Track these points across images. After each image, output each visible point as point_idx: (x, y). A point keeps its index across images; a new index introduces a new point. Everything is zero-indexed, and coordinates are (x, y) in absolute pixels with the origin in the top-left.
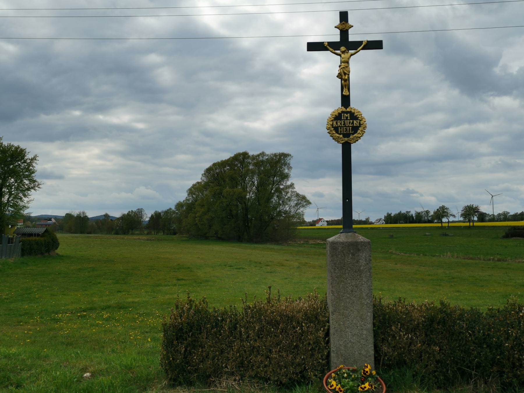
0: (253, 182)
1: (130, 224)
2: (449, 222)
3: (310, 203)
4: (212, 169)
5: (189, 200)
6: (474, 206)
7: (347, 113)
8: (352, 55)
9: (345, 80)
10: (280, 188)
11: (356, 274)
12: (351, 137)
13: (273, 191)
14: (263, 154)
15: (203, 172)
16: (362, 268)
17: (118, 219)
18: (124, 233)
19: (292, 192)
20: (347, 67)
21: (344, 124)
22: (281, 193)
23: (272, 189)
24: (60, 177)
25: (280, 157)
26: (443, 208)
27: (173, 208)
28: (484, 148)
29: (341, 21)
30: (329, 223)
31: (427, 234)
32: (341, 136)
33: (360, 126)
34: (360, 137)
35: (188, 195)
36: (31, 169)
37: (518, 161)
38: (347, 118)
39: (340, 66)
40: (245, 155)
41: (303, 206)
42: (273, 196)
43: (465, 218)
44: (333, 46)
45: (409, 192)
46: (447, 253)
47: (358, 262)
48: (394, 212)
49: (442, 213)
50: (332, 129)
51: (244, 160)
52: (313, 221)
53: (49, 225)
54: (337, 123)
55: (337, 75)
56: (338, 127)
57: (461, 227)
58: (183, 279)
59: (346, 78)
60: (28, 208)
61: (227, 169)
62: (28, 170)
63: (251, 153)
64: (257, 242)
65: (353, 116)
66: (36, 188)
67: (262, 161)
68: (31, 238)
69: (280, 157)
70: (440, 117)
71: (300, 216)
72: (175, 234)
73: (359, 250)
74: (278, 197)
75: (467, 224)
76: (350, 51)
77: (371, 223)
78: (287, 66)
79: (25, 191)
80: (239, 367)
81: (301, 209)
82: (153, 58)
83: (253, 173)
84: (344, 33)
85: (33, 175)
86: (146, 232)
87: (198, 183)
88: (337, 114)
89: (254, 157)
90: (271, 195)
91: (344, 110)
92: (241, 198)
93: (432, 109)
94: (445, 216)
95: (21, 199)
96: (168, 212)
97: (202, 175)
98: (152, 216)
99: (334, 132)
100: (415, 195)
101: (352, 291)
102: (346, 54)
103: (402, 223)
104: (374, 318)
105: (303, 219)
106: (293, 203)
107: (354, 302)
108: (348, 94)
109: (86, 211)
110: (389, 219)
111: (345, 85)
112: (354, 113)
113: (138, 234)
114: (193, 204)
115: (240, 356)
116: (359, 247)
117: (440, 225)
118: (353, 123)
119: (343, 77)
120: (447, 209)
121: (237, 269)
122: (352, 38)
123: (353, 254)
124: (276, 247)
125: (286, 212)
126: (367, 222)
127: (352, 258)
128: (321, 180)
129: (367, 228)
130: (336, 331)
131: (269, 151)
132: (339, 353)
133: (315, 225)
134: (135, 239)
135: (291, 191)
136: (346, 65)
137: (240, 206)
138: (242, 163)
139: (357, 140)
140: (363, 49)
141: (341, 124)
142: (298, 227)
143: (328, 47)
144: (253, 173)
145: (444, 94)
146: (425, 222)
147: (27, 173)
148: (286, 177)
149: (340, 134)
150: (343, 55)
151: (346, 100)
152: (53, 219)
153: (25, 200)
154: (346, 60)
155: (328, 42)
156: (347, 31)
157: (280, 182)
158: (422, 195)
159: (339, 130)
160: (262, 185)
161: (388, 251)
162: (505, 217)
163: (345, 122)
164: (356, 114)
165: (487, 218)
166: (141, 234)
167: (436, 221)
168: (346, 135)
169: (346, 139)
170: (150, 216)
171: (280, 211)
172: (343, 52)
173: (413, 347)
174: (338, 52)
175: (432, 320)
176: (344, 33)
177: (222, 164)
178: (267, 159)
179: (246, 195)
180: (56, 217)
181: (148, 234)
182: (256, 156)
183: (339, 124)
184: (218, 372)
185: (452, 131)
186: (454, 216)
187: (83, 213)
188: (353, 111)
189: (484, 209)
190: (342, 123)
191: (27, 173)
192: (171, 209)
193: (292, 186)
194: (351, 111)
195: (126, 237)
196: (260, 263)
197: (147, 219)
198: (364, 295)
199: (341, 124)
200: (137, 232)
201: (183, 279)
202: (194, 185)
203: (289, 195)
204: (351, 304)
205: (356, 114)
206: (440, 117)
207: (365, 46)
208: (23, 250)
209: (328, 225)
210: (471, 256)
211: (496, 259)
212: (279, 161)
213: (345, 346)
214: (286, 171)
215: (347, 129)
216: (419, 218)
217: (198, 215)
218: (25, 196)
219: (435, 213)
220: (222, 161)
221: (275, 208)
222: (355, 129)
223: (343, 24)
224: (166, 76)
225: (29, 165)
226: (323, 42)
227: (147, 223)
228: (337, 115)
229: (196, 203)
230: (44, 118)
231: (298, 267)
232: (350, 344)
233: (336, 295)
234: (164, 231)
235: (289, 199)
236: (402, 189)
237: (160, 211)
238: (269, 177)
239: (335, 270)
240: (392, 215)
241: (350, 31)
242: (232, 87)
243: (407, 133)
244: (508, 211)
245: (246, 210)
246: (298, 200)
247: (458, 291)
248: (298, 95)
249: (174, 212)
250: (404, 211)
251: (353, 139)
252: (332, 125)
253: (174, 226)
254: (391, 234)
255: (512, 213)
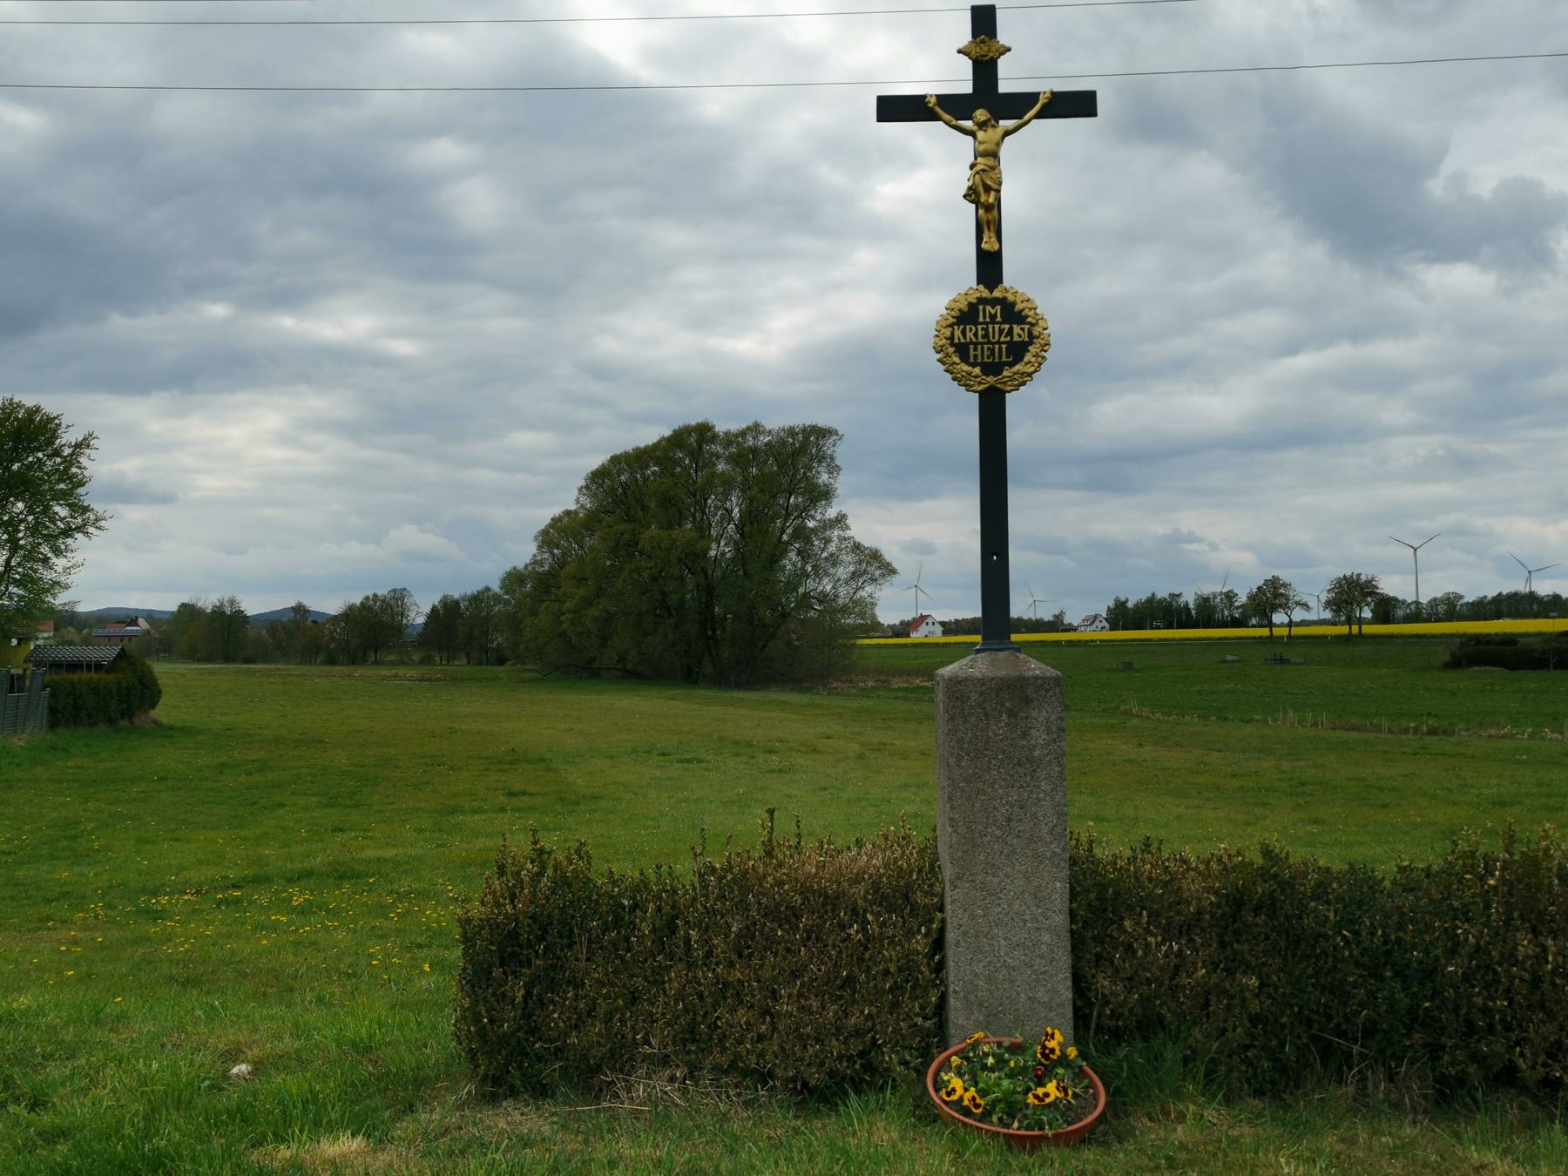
0: (729, 512)
1: (369, 633)
2: (1290, 624)
3: (893, 572)
4: (609, 474)
5: (541, 563)
6: (1363, 578)
7: (994, 302)
8: (1007, 133)
9: (988, 208)
10: (805, 527)
11: (1021, 770)
12: (1005, 373)
13: (785, 537)
14: (756, 429)
15: (583, 483)
16: (1036, 753)
17: (335, 619)
18: (353, 661)
19: (842, 539)
20: (993, 168)
21: (986, 336)
22: (808, 541)
23: (783, 532)
24: (164, 499)
25: (806, 438)
26: (1274, 583)
27: (496, 587)
28: (1394, 412)
29: (975, 35)
30: (948, 628)
31: (1229, 658)
32: (977, 370)
33: (1031, 343)
34: (1030, 375)
35: (540, 548)
36: (75, 475)
37: (1492, 448)
38: (993, 317)
39: (972, 167)
40: (704, 432)
41: (874, 580)
42: (786, 551)
43: (1337, 612)
44: (952, 108)
45: (1177, 539)
46: (1285, 712)
47: (1025, 735)
48: (1135, 597)
49: (1271, 597)
50: (951, 350)
51: (701, 448)
52: (902, 623)
53: (130, 638)
54: (964, 333)
55: (964, 191)
56: (966, 345)
57: (1325, 637)
58: (524, 793)
59: (991, 200)
60: (67, 587)
61: (654, 473)
62: (65, 475)
63: (721, 427)
64: (740, 685)
65: (1012, 313)
66: (91, 530)
67: (754, 450)
68: (75, 677)
69: (806, 438)
70: (1269, 322)
71: (864, 608)
72: (501, 661)
73: (1028, 701)
74: (799, 552)
75: (1344, 630)
76: (1002, 122)
77: (1070, 628)
78: (831, 176)
79: (57, 537)
80: (684, 1041)
81: (869, 589)
82: (445, 151)
83: (728, 483)
84: (985, 69)
85: (80, 490)
86: (416, 657)
87: (568, 513)
88: (963, 305)
89: (730, 439)
90: (781, 550)
91: (986, 293)
92: (694, 558)
93: (1247, 300)
94: (1280, 606)
95: (46, 560)
96: (478, 599)
97: (580, 490)
98: (434, 609)
99: (957, 360)
100: (1195, 546)
101: (1009, 820)
102: (990, 130)
103: (1158, 628)
104: (1073, 896)
105: (874, 616)
106: (842, 572)
107: (1014, 852)
108: (996, 247)
109: (238, 599)
110: (1121, 616)
111: (988, 222)
112: (1014, 304)
113: (393, 664)
114: (552, 574)
115: (686, 1010)
116: (1030, 691)
117: (1265, 632)
118: (1010, 332)
119: (983, 198)
120: (1285, 585)
121: (680, 761)
122: (1009, 82)
123: (1012, 714)
124: (795, 698)
125: (823, 598)
126: (1056, 625)
127: (1008, 725)
128: (928, 504)
129: (1057, 643)
130: (965, 934)
131: (775, 422)
132: (972, 998)
133: (908, 636)
134: (384, 678)
135: (839, 537)
136: (991, 162)
137: (690, 581)
138: (696, 454)
139: (1024, 383)
140: (1039, 116)
141: (976, 335)
142: (860, 642)
143: (938, 109)
144: (728, 483)
145: (1283, 257)
146: (1224, 624)
147: (62, 486)
148: (823, 495)
149: (974, 365)
150: (980, 135)
151: (989, 265)
152: (141, 621)
153: (60, 563)
154: (991, 147)
155: (938, 97)
156: (993, 64)
157: (805, 509)
158: (1214, 547)
159: (972, 353)
160: (753, 520)
161: (1117, 708)
162: (1450, 608)
163: (986, 330)
164: (1019, 307)
165: (1400, 613)
166: (403, 663)
167: (1254, 621)
168: (992, 369)
169: (991, 379)
170: (427, 609)
171: (805, 595)
172: (982, 125)
173: (1183, 979)
174: (968, 124)
175: (1237, 901)
176: (985, 69)
177: (640, 458)
178: (768, 444)
179: (709, 549)
180: (150, 616)
181: (422, 662)
182: (737, 436)
183: (969, 335)
184: (622, 1057)
185: (1304, 362)
186: (1306, 606)
187: (232, 602)
188: (1011, 298)
189: (1393, 585)
190: (980, 333)
191: (62, 486)
192: (488, 589)
193: (840, 520)
194: (1005, 299)
195: (358, 671)
196: (750, 745)
197: (421, 620)
198: (1044, 829)
199: (976, 335)
200: (392, 657)
201: (524, 793)
202: (555, 521)
203: (832, 548)
204: (1008, 856)
205: (1019, 307)
206: (1269, 322)
207: (1044, 106)
208: (52, 711)
209: (945, 633)
210: (1354, 721)
211: (1425, 729)
212: (803, 449)
213: (990, 979)
214: (824, 477)
215: (992, 351)
216: (1206, 613)
217: (568, 605)
218: (58, 552)
219: (1252, 598)
220: (637, 450)
221: (792, 586)
222: (1018, 351)
223: (983, 42)
224: (479, 203)
225: (71, 460)
226: (925, 97)
227: (420, 630)
228: (966, 309)
229: (563, 573)
230: (120, 325)
231: (861, 756)
232: (1004, 971)
233: (962, 830)
234: (468, 655)
235: (834, 560)
236: (1160, 529)
237: (456, 596)
238: (774, 496)
239: (959, 758)
240: (1130, 605)
241: (1002, 63)
242: (671, 236)
243: (1178, 368)
244: (1460, 591)
245: (709, 591)
246: (860, 563)
247: (1316, 822)
248: (865, 257)
249: (497, 598)
250: (1162, 594)
251: (1011, 378)
252: (951, 338)
253: (499, 639)
254: (1127, 659)
255: (1470, 598)
